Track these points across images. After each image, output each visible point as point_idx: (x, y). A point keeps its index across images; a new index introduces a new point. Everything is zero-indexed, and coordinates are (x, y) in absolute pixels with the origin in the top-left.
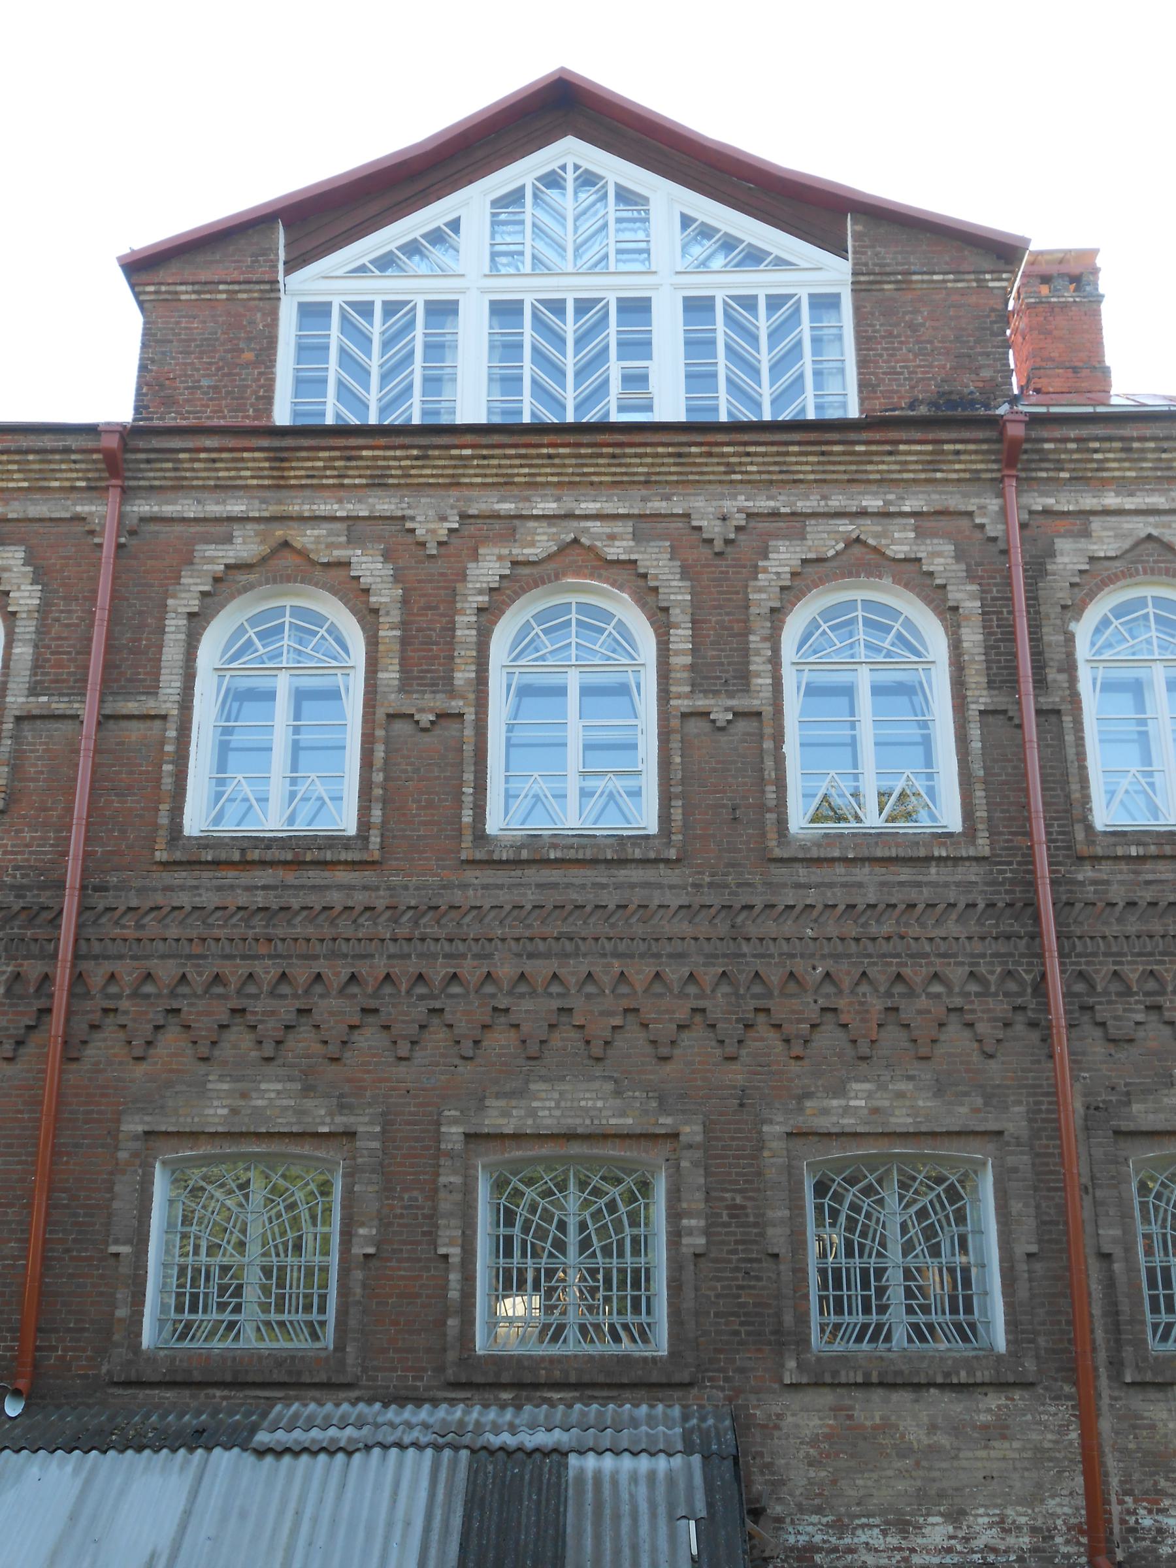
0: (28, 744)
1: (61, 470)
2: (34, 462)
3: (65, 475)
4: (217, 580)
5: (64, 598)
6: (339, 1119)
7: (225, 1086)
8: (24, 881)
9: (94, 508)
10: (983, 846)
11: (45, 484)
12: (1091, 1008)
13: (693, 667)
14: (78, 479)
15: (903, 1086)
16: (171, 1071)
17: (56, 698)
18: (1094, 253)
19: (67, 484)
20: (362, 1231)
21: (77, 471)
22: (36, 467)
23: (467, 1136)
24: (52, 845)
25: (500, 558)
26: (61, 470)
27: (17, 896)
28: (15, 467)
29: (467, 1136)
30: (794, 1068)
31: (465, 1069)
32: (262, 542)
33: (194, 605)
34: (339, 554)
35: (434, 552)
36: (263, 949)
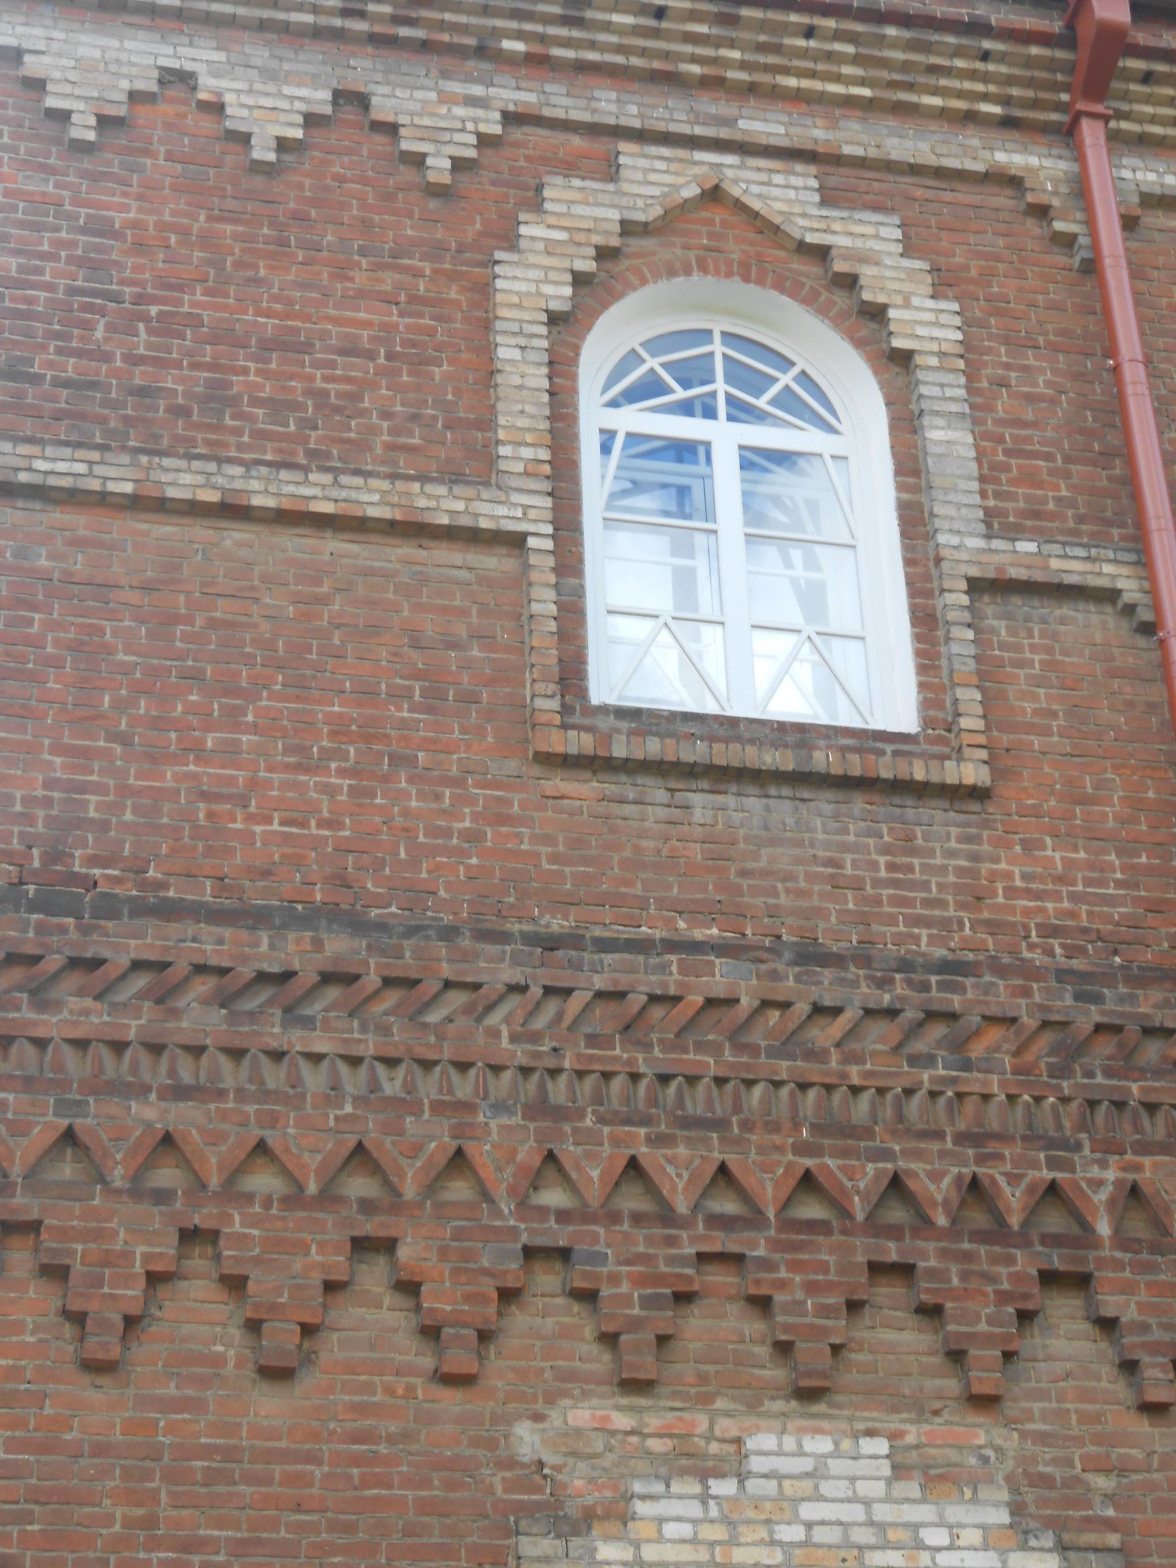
0: (1003, 646)
1: (947, 72)
2: (894, 44)
3: (956, 84)
4: (604, 254)
5: (1006, 341)
8: (1075, 963)
9: (1034, 161)
11: (912, 98)
12: (212, 1236)
14: (985, 97)
17: (1056, 549)
19: (961, 105)
21: (986, 78)
22: (898, 55)
24: (1119, 884)
26: (947, 72)
28: (850, 49)
35: (91, 136)
36: (230, 1075)
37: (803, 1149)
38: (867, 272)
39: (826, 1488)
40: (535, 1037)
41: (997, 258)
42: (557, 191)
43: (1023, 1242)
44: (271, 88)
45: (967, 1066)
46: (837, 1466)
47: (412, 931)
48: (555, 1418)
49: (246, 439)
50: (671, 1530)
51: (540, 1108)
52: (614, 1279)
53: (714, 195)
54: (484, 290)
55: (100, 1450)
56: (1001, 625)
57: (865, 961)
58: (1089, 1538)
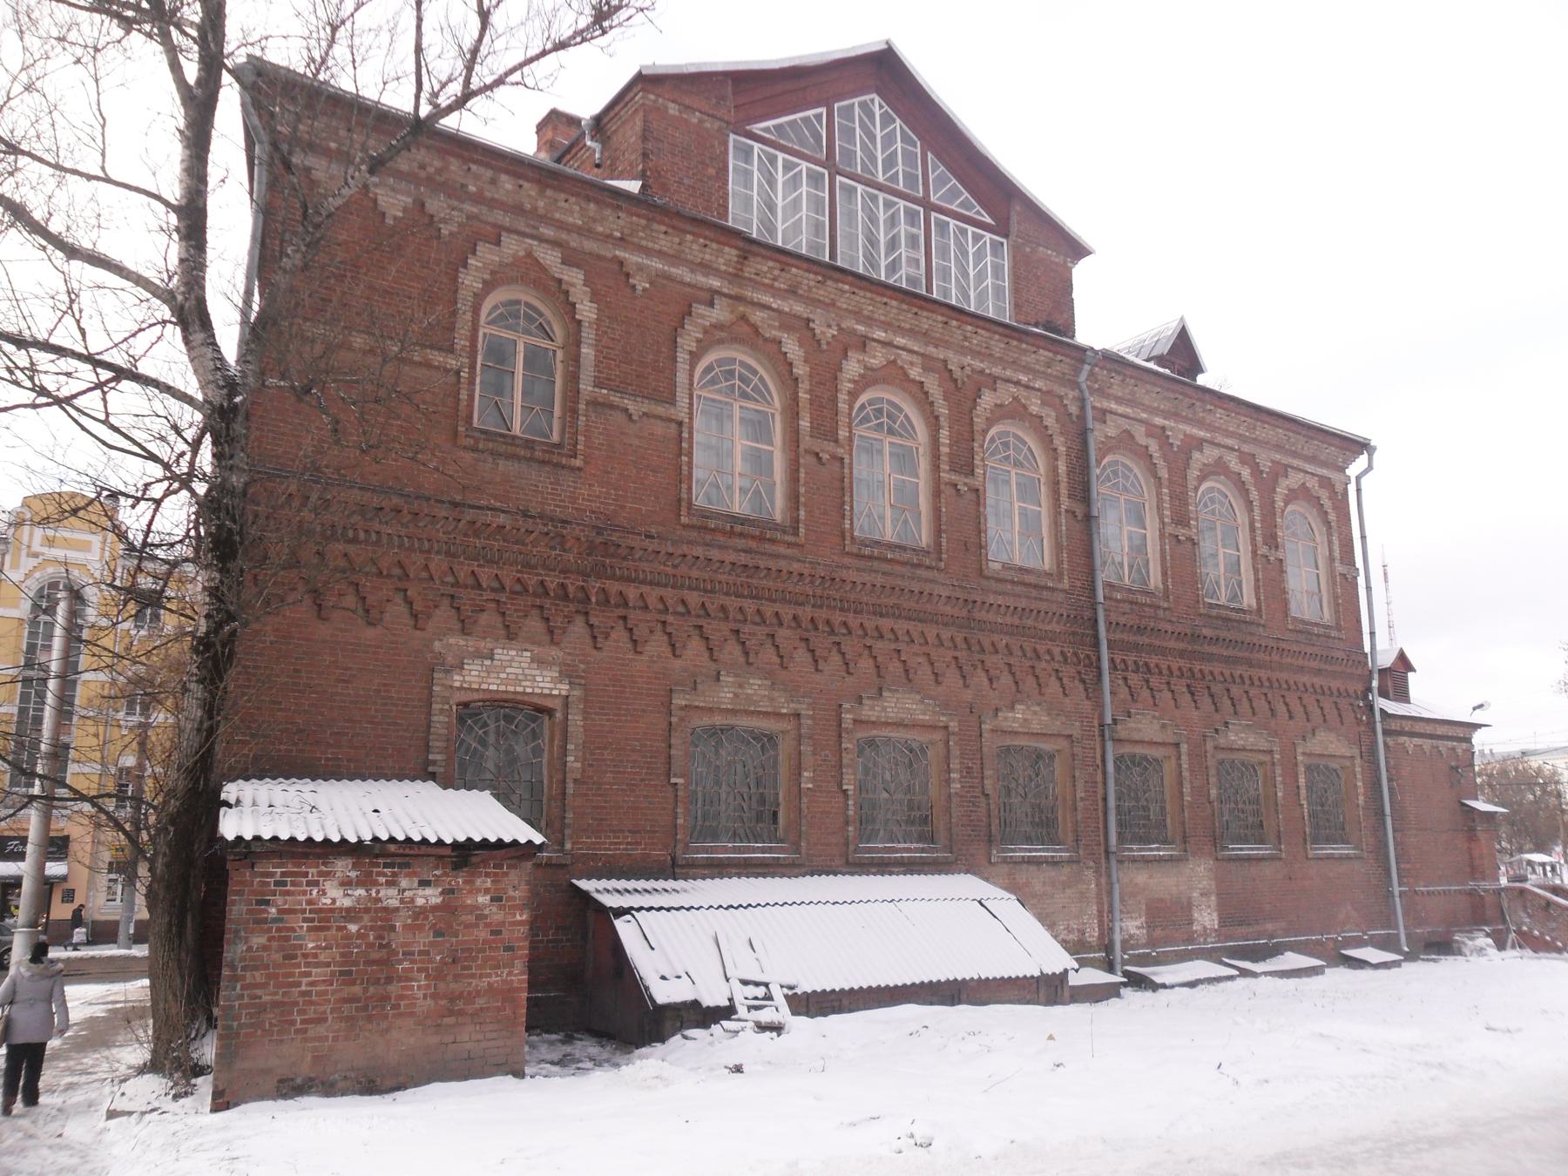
6: (792, 705)
7: (731, 679)
10: (1066, 584)
13: (950, 454)
15: (1037, 708)
16: (695, 666)
18: (1078, 250)
20: (806, 774)
23: (855, 721)
25: (859, 361)
27: (598, 533)
29: (855, 721)
30: (991, 693)
31: (849, 679)
32: (732, 312)
33: (693, 346)
34: (775, 333)
37: (518, 571)
38: (572, 290)
39: (513, 664)
40: (450, 533)
41: (610, 288)
42: (482, 248)
43: (573, 602)
44: (392, 194)
45: (565, 551)
46: (516, 659)
47: (417, 498)
48: (445, 642)
49: (237, 1003)
50: (473, 673)
51: (448, 553)
52: (465, 604)
53: (529, 254)
54: (455, 279)
55: (324, 641)
56: (593, 415)
57: (541, 518)
58: (577, 681)
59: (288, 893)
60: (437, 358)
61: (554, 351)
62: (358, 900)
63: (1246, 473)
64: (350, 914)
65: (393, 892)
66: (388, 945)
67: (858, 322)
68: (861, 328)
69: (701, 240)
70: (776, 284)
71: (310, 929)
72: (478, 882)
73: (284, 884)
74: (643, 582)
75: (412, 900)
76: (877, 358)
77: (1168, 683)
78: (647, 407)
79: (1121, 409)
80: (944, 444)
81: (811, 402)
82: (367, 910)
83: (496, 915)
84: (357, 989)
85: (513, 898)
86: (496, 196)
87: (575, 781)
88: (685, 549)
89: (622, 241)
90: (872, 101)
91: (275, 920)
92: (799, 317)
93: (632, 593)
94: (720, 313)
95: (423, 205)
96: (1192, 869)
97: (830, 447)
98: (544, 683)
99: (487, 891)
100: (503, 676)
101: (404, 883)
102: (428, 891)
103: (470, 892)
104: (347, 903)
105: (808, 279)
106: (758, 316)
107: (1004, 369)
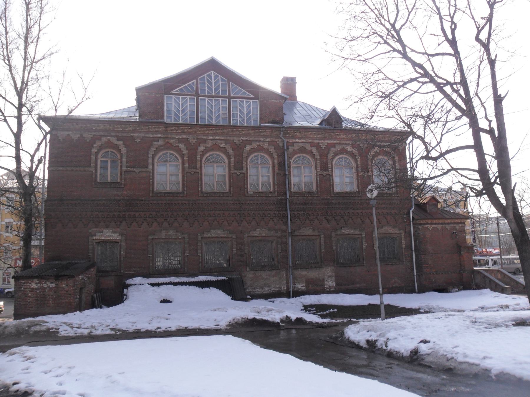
6: (182, 236)
13: (234, 166)
25: (203, 146)
38: (120, 146)
53: (109, 140)
59: (25, 285)
60: (87, 169)
61: (118, 161)
62: (39, 286)
63: (355, 151)
64: (37, 289)
65: (46, 285)
66: (45, 294)
67: (204, 136)
68: (205, 137)
69: (153, 126)
70: (178, 132)
71: (30, 292)
72: (63, 282)
73: (24, 284)
74: (140, 211)
75: (49, 286)
76: (210, 144)
77: (317, 218)
78: (140, 170)
79: (300, 141)
80: (232, 163)
81: (188, 160)
82: (40, 288)
83: (67, 288)
84: (39, 302)
85: (71, 285)
86: (100, 129)
87: (124, 257)
88: (151, 202)
89: (134, 131)
90: (211, 73)
91: (23, 290)
92: (185, 139)
93: (137, 214)
94: (161, 143)
95: (82, 135)
96: (325, 270)
97: (195, 170)
98: (115, 236)
99: (65, 284)
100: (105, 236)
101: (48, 283)
102: (53, 284)
103: (61, 284)
104: (37, 287)
105: (186, 129)
106: (172, 141)
107: (255, 138)
